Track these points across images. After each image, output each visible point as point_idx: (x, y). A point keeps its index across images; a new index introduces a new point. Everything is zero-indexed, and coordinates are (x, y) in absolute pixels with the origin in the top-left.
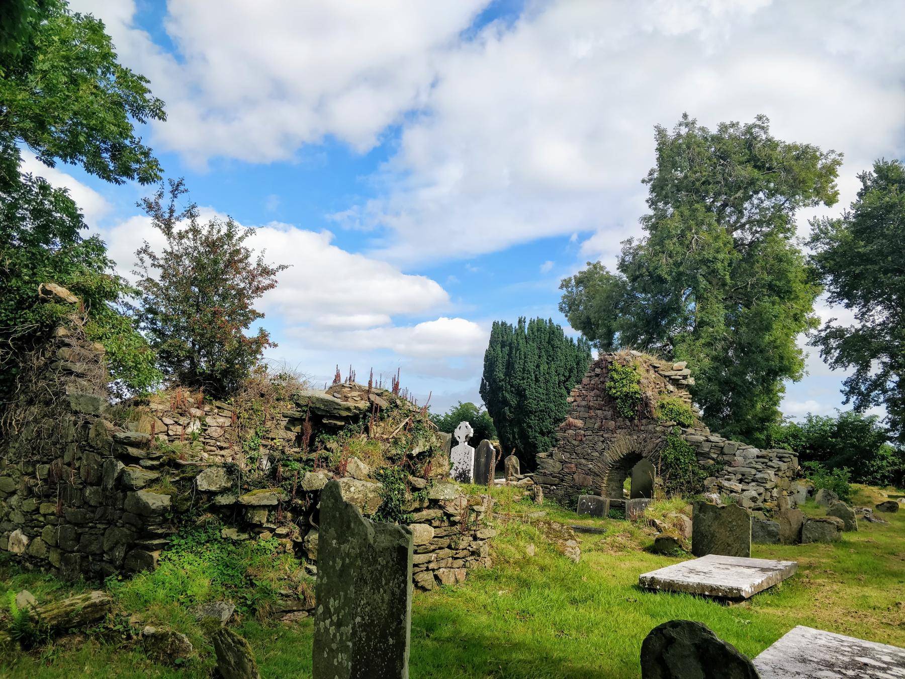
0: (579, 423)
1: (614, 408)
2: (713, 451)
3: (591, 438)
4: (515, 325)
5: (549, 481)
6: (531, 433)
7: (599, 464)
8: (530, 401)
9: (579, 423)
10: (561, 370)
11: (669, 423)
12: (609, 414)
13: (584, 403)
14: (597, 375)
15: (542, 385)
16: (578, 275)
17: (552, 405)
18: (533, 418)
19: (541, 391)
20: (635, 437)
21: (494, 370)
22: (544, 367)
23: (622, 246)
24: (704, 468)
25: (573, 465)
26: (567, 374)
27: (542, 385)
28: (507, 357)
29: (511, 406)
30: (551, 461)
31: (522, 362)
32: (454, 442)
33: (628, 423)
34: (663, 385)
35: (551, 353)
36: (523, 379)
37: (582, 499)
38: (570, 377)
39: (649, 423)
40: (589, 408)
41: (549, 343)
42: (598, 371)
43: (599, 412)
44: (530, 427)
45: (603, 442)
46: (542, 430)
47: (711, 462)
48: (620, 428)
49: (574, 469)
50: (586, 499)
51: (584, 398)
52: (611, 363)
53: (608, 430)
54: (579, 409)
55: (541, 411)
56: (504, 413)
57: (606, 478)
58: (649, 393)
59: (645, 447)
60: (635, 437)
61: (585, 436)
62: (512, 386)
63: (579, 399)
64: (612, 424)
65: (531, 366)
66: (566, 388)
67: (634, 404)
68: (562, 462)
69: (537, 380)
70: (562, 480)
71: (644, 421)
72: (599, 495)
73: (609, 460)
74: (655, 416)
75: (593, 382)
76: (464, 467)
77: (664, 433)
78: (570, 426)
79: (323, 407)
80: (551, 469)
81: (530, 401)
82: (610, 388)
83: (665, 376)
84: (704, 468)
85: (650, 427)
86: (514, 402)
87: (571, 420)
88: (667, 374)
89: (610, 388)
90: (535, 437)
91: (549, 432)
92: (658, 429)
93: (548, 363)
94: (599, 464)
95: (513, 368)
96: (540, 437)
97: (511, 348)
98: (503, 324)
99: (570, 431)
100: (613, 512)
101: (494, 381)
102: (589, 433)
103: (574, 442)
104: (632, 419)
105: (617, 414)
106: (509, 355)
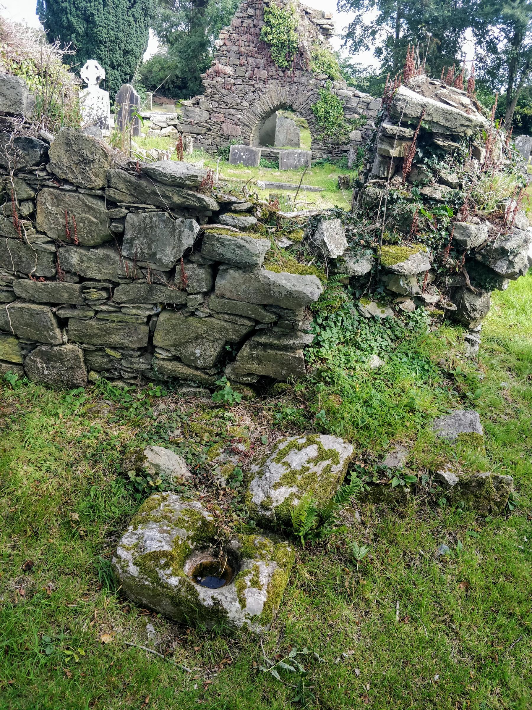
0: (229, 70)
2: (359, 106)
3: (241, 87)
5: (195, 131)
7: (249, 115)
8: (100, 28)
9: (229, 70)
13: (235, 48)
14: (250, 17)
15: (111, 11)
18: (103, 48)
19: (111, 18)
20: (288, 89)
24: (350, 122)
25: (222, 115)
27: (111, 11)
29: (78, 34)
33: (281, 74)
34: (315, 35)
37: (234, 149)
39: (303, 75)
40: (240, 54)
42: (251, 11)
43: (250, 59)
45: (254, 92)
47: (357, 116)
49: (223, 119)
50: (238, 149)
51: (235, 42)
53: (260, 80)
54: (229, 55)
55: (111, 41)
58: (306, 44)
60: (288, 89)
61: (235, 85)
63: (229, 43)
64: (264, 74)
66: (134, 16)
70: (209, 130)
71: (297, 73)
72: (248, 144)
73: (259, 111)
74: (309, 68)
75: (245, 24)
76: (99, 114)
78: (218, 73)
79: (443, 122)
81: (100, 28)
83: (317, 25)
84: (350, 122)
85: (303, 79)
86: (81, 29)
87: (220, 66)
88: (319, 22)
89: (266, 34)
91: (120, 65)
92: (311, 82)
94: (249, 115)
99: (219, 79)
100: (266, 162)
102: (239, 82)
103: (223, 91)
105: (271, 63)
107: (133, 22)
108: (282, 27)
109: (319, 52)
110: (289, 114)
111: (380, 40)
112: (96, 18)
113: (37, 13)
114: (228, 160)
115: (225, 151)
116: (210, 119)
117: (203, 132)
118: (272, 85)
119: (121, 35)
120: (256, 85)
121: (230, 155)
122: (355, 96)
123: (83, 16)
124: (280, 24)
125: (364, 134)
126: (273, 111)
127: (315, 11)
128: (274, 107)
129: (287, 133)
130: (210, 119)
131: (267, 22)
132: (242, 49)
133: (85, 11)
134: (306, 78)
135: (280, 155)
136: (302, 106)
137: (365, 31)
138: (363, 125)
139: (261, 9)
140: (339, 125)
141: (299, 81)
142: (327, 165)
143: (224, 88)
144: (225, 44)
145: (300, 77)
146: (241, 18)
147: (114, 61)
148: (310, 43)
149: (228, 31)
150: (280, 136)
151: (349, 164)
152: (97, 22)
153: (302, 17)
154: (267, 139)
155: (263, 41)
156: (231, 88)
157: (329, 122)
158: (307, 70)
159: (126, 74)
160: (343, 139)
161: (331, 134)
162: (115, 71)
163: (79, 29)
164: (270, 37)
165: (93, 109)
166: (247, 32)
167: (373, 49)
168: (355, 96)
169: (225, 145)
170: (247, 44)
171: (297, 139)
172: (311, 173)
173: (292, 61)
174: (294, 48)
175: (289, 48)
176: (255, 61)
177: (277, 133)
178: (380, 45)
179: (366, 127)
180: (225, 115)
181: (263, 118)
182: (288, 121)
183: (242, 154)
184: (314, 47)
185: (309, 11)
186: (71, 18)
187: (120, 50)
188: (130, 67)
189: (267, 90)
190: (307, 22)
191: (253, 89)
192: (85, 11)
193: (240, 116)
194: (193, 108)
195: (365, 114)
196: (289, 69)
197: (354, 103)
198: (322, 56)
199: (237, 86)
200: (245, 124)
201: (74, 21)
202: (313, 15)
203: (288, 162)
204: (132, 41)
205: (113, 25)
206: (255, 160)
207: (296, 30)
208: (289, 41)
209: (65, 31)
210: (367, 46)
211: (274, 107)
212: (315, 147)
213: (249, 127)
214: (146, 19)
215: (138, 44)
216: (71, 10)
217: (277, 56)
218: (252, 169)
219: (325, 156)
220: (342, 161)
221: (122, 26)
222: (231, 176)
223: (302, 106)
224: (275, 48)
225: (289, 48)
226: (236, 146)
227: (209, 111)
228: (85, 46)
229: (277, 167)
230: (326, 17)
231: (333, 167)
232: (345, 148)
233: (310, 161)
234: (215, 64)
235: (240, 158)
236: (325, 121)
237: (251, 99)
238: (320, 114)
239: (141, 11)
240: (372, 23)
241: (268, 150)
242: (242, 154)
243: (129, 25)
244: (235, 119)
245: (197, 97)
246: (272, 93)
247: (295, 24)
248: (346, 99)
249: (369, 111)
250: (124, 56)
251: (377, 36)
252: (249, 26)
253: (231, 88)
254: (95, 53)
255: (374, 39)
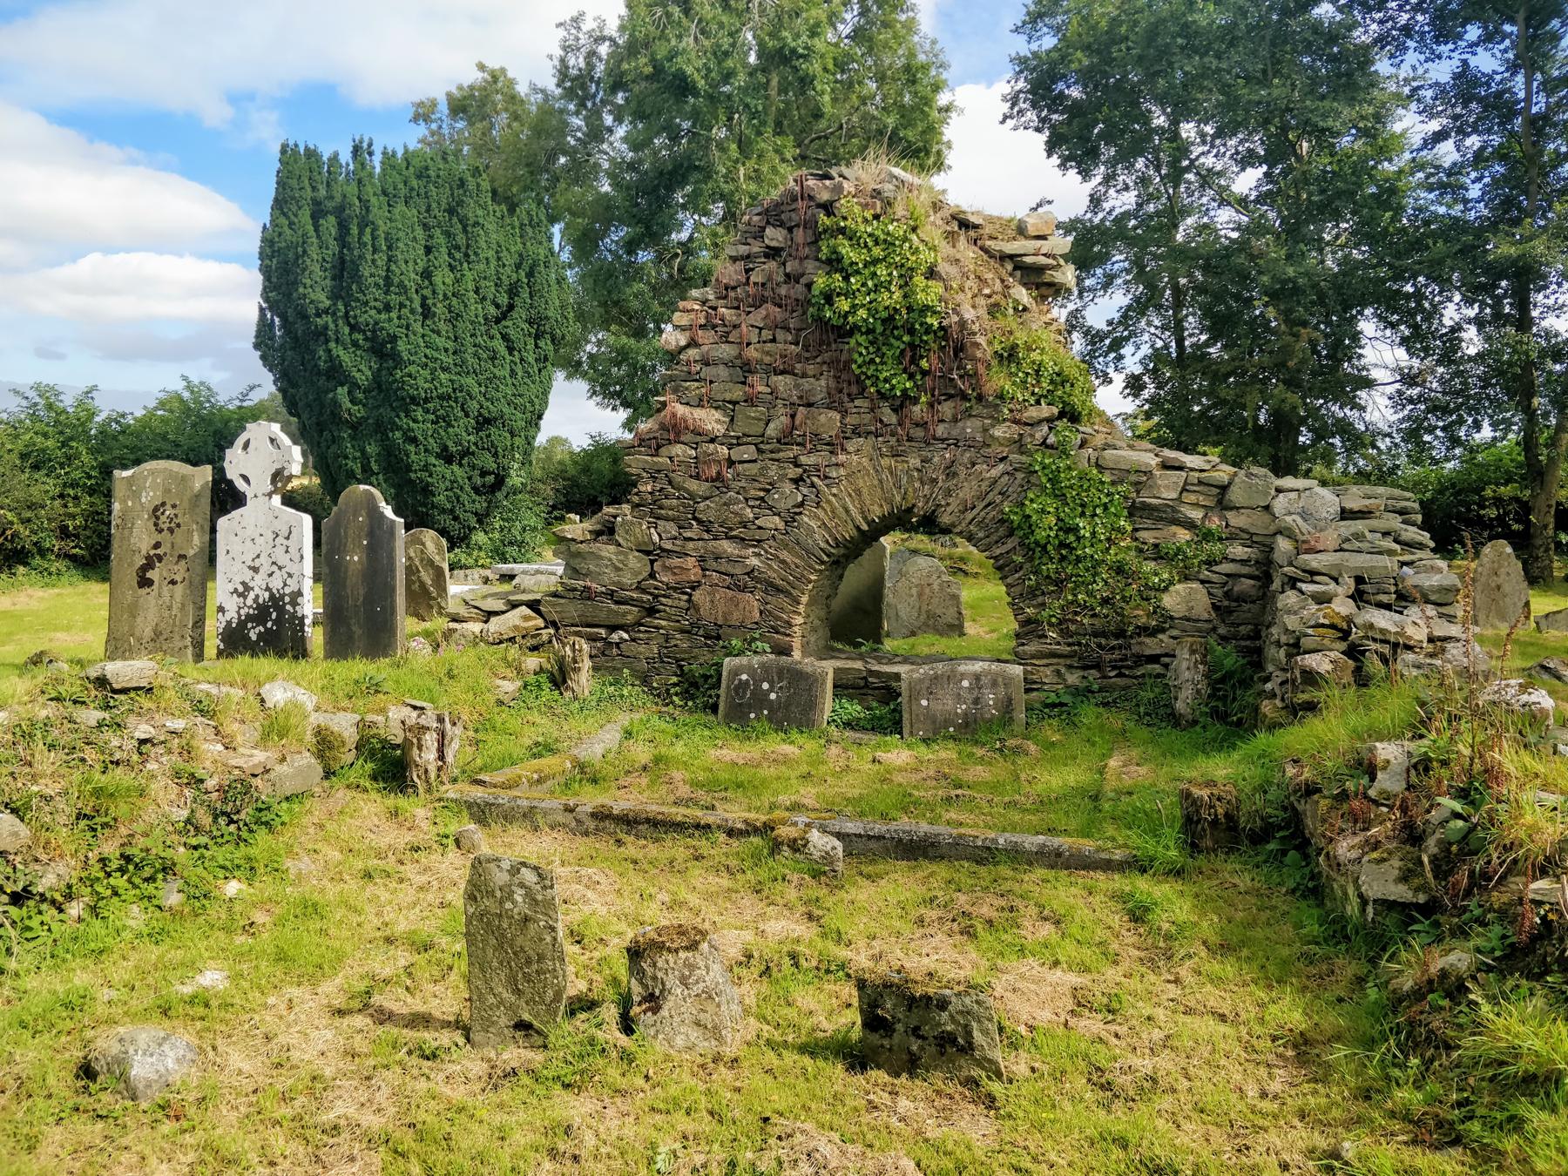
0: (711, 420)
1: (841, 367)
3: (753, 469)
4: (345, 157)
6: (415, 457)
7: (784, 555)
8: (412, 369)
9: (711, 420)
10: (489, 289)
11: (1033, 413)
12: (819, 387)
13: (726, 351)
14: (773, 253)
15: (442, 326)
16: (454, 91)
17: (470, 381)
18: (419, 414)
19: (440, 342)
20: (915, 462)
21: (296, 283)
22: (443, 278)
23: (561, 33)
25: (691, 562)
26: (504, 300)
27: (442, 326)
28: (334, 247)
29: (354, 385)
30: (608, 551)
31: (381, 260)
32: (226, 497)
33: (889, 417)
34: (998, 286)
35: (461, 239)
36: (388, 308)
37: (735, 673)
38: (511, 307)
40: (746, 368)
41: (451, 211)
42: (775, 236)
43: (781, 382)
44: (414, 440)
45: (797, 481)
46: (445, 448)
47: (1183, 535)
48: (856, 432)
49: (694, 574)
50: (750, 670)
52: (828, 208)
54: (707, 372)
55: (441, 397)
56: (336, 404)
57: (805, 599)
58: (969, 314)
59: (948, 493)
60: (915, 462)
62: (354, 328)
64: (829, 421)
65: (411, 278)
66: (505, 337)
67: (914, 352)
68: (651, 552)
69: (427, 313)
70: (652, 612)
71: (947, 409)
73: (820, 538)
76: (276, 584)
77: (1019, 444)
80: (610, 576)
81: (412, 369)
82: (829, 298)
83: (1004, 257)
85: (970, 427)
87: (681, 410)
89: (829, 298)
90: (426, 468)
93: (452, 268)
94: (784, 555)
95: (356, 277)
96: (440, 467)
97: (343, 227)
98: (311, 154)
99: (678, 450)
100: (854, 709)
101: (304, 316)
102: (748, 452)
103: (693, 485)
104: (902, 403)
105: (850, 385)
106: (342, 239)
107: (502, 350)
108: (882, 271)
109: (1021, 337)
110: (920, 541)
111: (1133, 359)
112: (402, 346)
113: (257, 346)
114: (714, 709)
115: (706, 677)
116: (652, 576)
117: (630, 619)
118: (858, 454)
119: (470, 381)
120: (803, 459)
121: (722, 691)
122: (1166, 466)
123: (368, 345)
124: (875, 262)
125: (1218, 592)
126: (869, 537)
127: (991, 220)
128: (870, 523)
129: (920, 595)
130: (652, 576)
131: (829, 262)
132: (752, 353)
133: (374, 331)
134: (978, 423)
135: (904, 685)
136: (969, 516)
137: (1093, 344)
138: (1210, 563)
139: (810, 224)
140: (1119, 570)
141: (955, 433)
142: (1089, 714)
143: (697, 477)
144: (693, 343)
145: (955, 420)
146: (742, 258)
147: (450, 444)
148: (983, 312)
149: (704, 303)
150: (899, 602)
151: (1180, 706)
152: (405, 356)
153: (950, 236)
154: (857, 622)
155: (820, 321)
156: (719, 477)
157: (1078, 560)
158: (980, 398)
159: (483, 474)
160: (1140, 615)
161: (1090, 601)
162: (455, 468)
163: (358, 375)
164: (844, 305)
165: (255, 570)
166: (764, 300)
167: (1119, 380)
168: (1166, 466)
169: (705, 657)
170: (767, 335)
171: (952, 611)
172: (1032, 748)
173: (925, 373)
174: (928, 329)
175: (911, 331)
176: (797, 386)
177: (889, 597)
178: (1138, 370)
179: (1226, 568)
180: (702, 559)
181: (836, 563)
182: (922, 561)
183: (765, 686)
184: (1001, 323)
185: (974, 219)
186: (338, 351)
187: (467, 416)
188: (496, 455)
189: (842, 471)
190: (967, 252)
191: (793, 472)
192: (374, 331)
193: (754, 561)
194: (595, 547)
195: (1215, 523)
196: (916, 401)
197: (1166, 488)
198: (1029, 349)
199: (740, 467)
200: (772, 585)
201: (345, 357)
202: (987, 230)
203: (937, 707)
204: (500, 395)
205: (448, 360)
206: (812, 705)
207: (931, 273)
208: (910, 309)
209: (322, 381)
210: (1106, 374)
211: (870, 523)
212: (1031, 648)
213: (788, 594)
214: (541, 343)
215: (518, 401)
216: (337, 332)
217: (872, 361)
218: (801, 739)
219: (1073, 678)
220: (1147, 695)
221: (471, 360)
222: (713, 785)
223: (969, 516)
224: (862, 339)
225: (911, 331)
226: (743, 660)
227: (648, 553)
228: (375, 413)
229: (895, 726)
230: (1032, 231)
231: (1116, 720)
232: (1151, 646)
233: (1021, 699)
234: (664, 404)
235: (760, 700)
236: (1063, 558)
237: (790, 503)
238: (1041, 535)
239: (525, 326)
240: (1110, 323)
241: (858, 665)
242: (765, 686)
243: (493, 359)
244: (738, 570)
245: (606, 510)
246: (860, 479)
247: (926, 256)
248: (1133, 478)
249: (1229, 515)
250: (478, 430)
251: (1127, 350)
252: (770, 279)
253: (719, 477)
254: (399, 428)
255: (1120, 358)
